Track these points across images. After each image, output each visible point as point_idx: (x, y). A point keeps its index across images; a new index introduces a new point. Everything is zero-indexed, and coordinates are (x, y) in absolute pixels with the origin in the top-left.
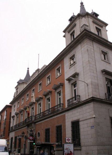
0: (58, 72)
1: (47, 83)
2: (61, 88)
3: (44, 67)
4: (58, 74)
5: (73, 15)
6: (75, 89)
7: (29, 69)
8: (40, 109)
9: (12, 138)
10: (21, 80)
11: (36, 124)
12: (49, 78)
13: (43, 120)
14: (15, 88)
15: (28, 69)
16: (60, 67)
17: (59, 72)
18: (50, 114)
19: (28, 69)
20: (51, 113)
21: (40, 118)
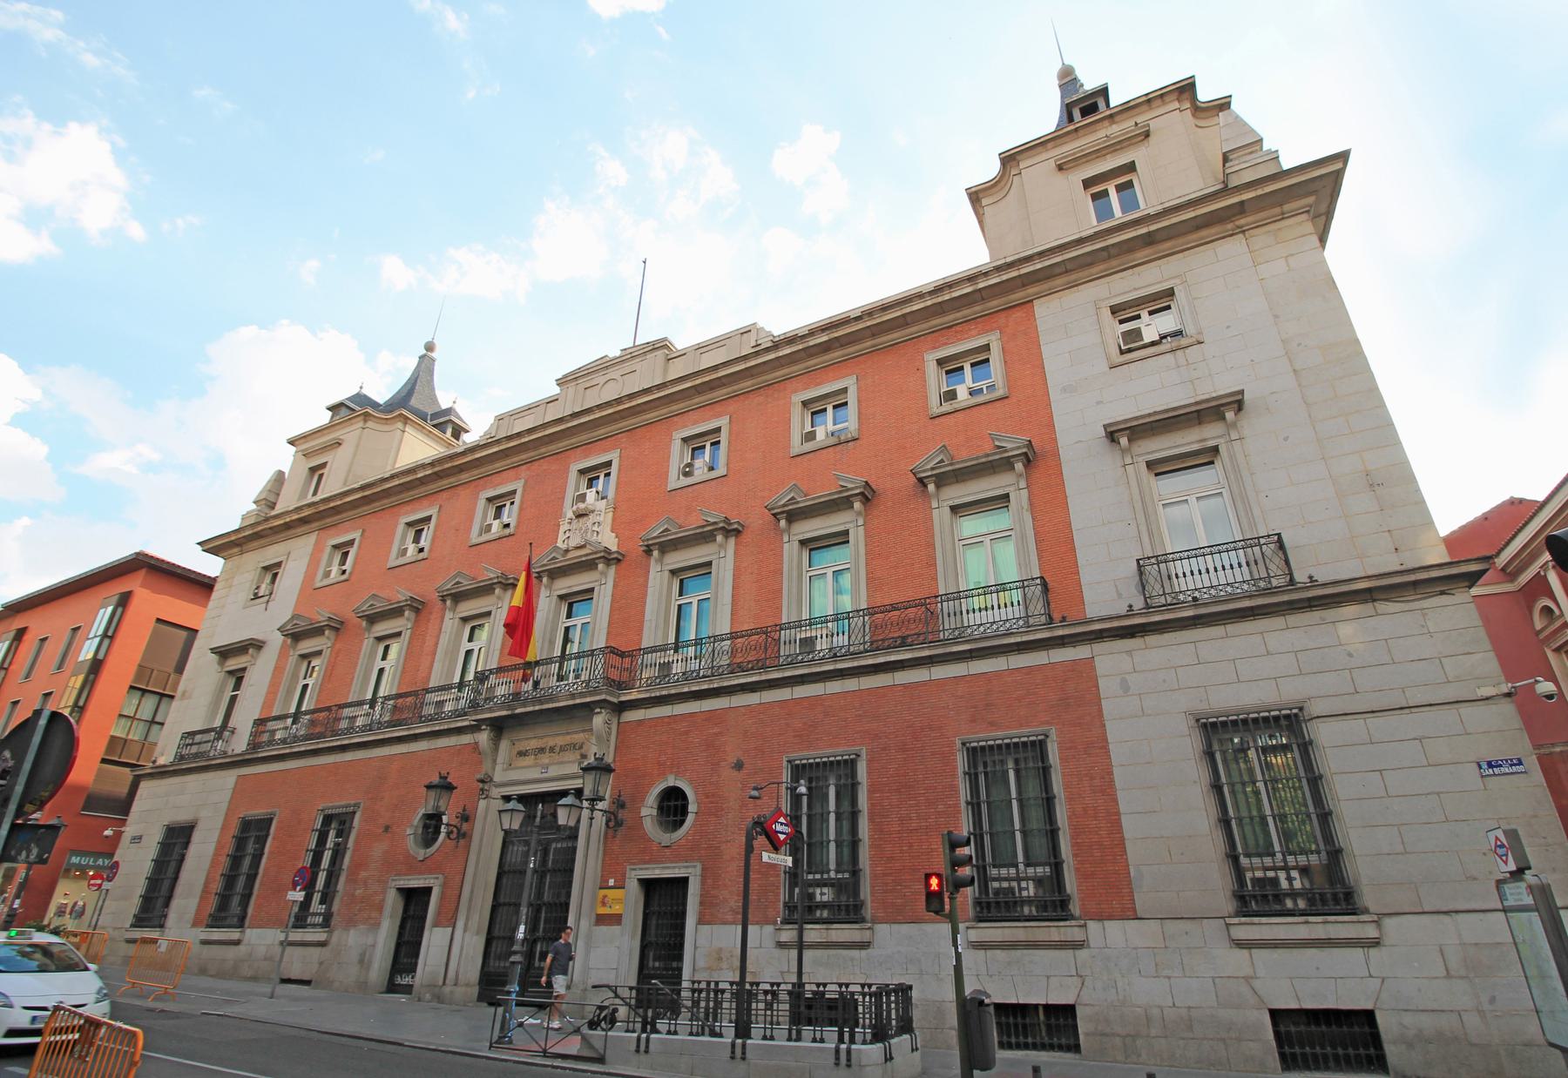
0: (338, 557)
1: (327, 574)
2: (859, 514)
3: (746, 332)
4: (412, 549)
5: (1060, 66)
6: (469, 646)
7: (433, 355)
8: (381, 671)
9: (178, 837)
10: (361, 399)
11: (632, 716)
12: (417, 527)
13: (753, 691)
14: (292, 442)
15: (430, 347)
16: (429, 519)
17: (343, 562)
18: (296, 739)
19: (430, 347)
20: (307, 738)
21: (368, 728)
